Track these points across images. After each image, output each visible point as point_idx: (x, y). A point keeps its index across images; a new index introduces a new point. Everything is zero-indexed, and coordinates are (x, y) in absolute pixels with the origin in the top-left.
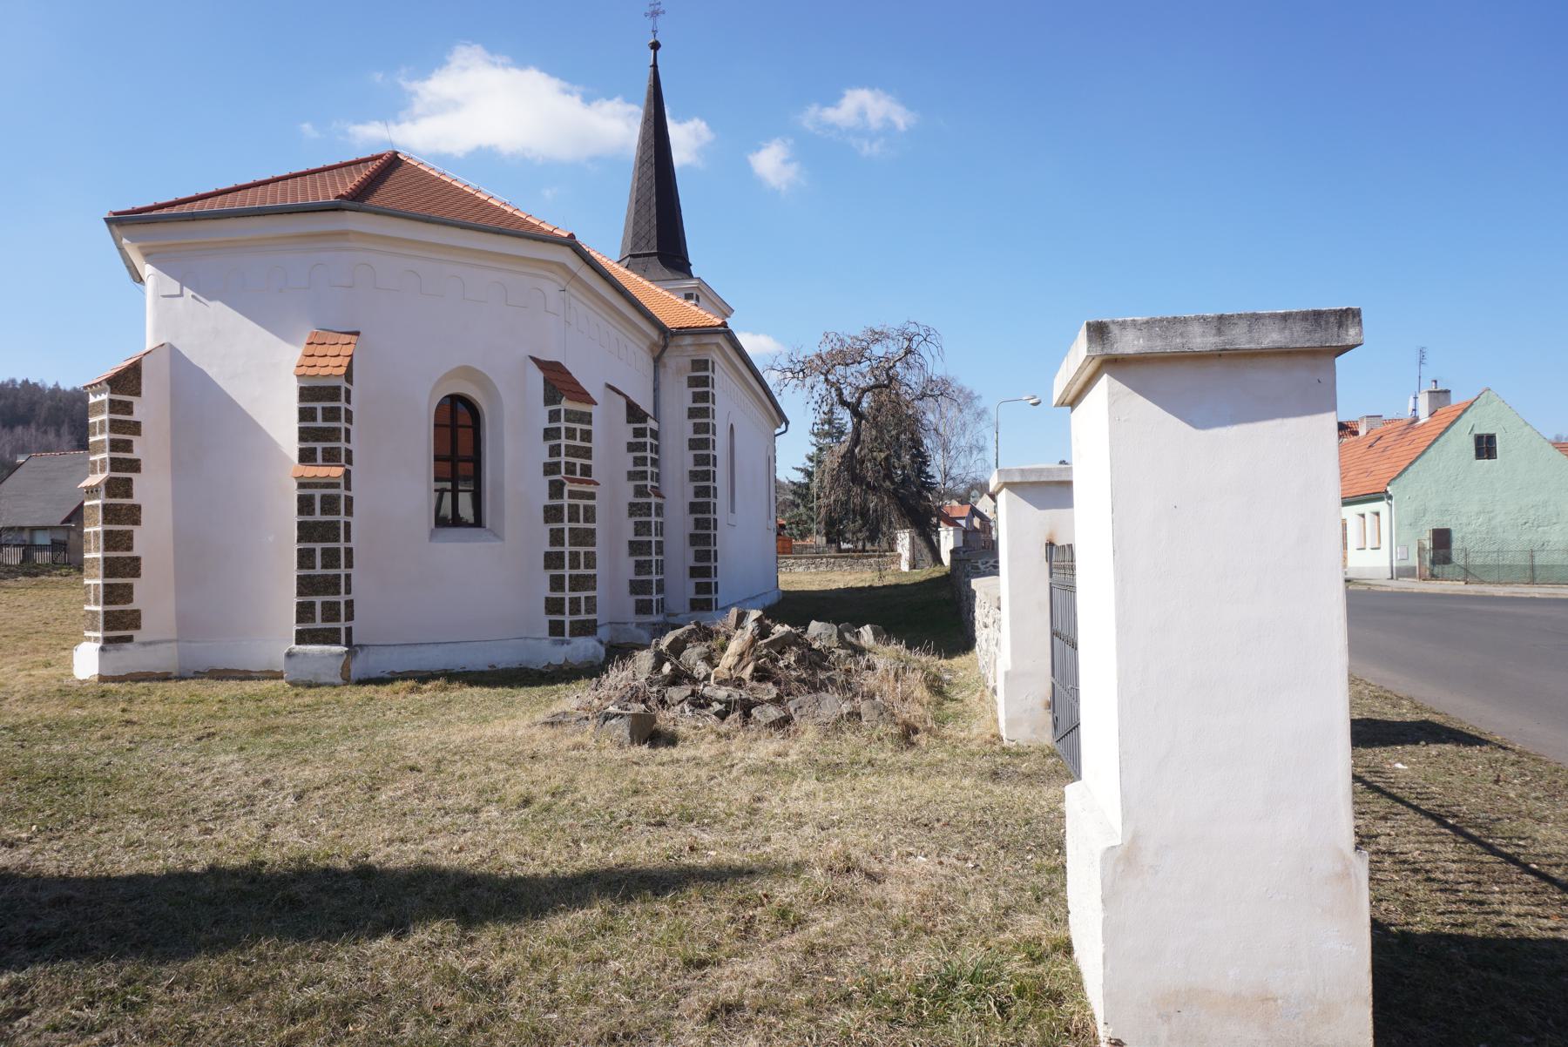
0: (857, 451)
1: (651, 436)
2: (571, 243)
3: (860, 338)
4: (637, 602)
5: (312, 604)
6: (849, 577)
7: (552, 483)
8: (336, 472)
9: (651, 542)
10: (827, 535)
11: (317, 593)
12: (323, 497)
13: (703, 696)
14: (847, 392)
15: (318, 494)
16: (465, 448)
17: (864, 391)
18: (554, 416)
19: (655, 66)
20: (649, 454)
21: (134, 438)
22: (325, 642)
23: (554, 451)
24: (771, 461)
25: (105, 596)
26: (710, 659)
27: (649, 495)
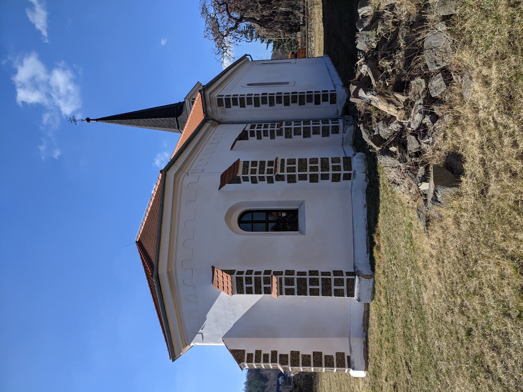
0: (258, 19)
1: (254, 128)
2: (164, 172)
3: (206, 19)
4: (333, 133)
5: (335, 290)
6: (317, 20)
7: (277, 180)
8: (275, 279)
9: (304, 127)
10: (296, 32)
11: (330, 288)
12: (286, 285)
13: (418, 129)
14: (231, 25)
15: (284, 287)
16: (263, 217)
17: (230, 17)
18: (246, 179)
19: (97, 120)
20: (262, 129)
21: (263, 353)
22: (353, 285)
23: (262, 179)
24: (264, 63)
25: (330, 367)
26: (388, 120)
27: (282, 129)
